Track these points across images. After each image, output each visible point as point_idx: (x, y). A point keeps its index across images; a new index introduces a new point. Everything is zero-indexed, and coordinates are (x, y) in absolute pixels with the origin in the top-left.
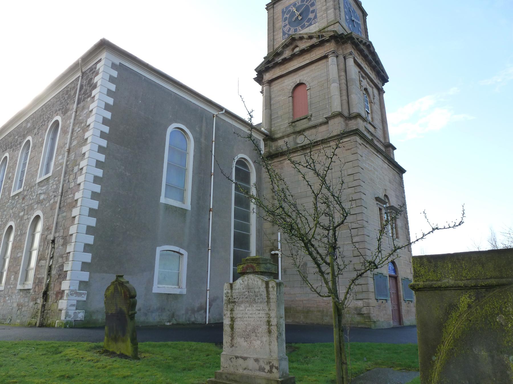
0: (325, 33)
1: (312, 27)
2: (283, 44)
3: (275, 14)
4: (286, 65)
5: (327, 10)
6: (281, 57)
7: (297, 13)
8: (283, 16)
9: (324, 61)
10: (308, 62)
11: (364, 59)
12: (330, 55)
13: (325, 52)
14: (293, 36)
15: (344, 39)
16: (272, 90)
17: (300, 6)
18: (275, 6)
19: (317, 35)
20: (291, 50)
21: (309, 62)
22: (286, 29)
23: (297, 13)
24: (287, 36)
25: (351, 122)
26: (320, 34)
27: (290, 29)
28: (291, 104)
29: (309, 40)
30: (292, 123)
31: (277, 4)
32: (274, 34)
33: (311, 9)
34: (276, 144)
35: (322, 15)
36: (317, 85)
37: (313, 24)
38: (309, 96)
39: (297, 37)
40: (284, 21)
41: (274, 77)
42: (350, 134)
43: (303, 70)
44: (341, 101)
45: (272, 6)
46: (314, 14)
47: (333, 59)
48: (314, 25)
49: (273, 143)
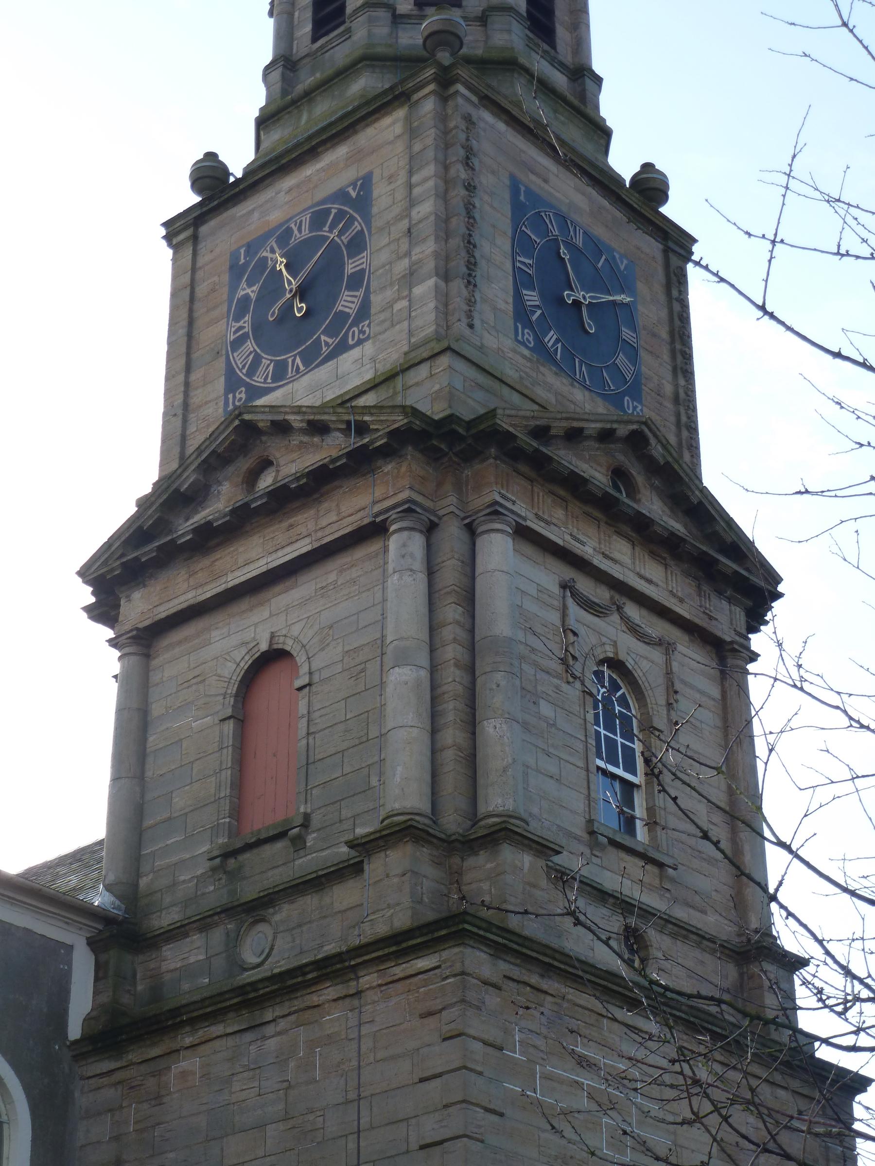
0: (372, 414)
1: (347, 360)
2: (199, 455)
3: (200, 274)
4: (218, 555)
5: (410, 278)
6: (197, 512)
7: (291, 283)
8: (233, 288)
9: (374, 547)
10: (303, 547)
11: (597, 514)
12: (394, 521)
13: (375, 503)
14: (247, 417)
15: (462, 438)
16: (155, 677)
17: (310, 244)
18: (204, 229)
19: (342, 421)
20: (240, 479)
21: (309, 548)
22: (241, 359)
23: (290, 283)
24: (243, 396)
25: (471, 862)
26: (352, 418)
27: (257, 361)
28: (228, 755)
29: (316, 439)
30: (227, 855)
31: (213, 223)
32: (193, 377)
33: (350, 268)
34: (152, 965)
35: (390, 305)
36: (339, 668)
37: (352, 347)
38: (303, 723)
39: (262, 420)
40: (237, 319)
41: (163, 615)
42: (436, 935)
43: (288, 583)
44: (434, 751)
45: (189, 233)
46: (360, 293)
47: (404, 545)
48: (355, 353)
49: (141, 958)
